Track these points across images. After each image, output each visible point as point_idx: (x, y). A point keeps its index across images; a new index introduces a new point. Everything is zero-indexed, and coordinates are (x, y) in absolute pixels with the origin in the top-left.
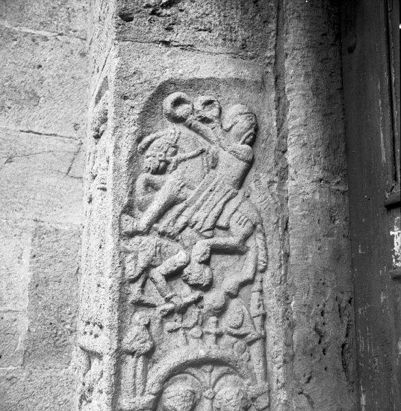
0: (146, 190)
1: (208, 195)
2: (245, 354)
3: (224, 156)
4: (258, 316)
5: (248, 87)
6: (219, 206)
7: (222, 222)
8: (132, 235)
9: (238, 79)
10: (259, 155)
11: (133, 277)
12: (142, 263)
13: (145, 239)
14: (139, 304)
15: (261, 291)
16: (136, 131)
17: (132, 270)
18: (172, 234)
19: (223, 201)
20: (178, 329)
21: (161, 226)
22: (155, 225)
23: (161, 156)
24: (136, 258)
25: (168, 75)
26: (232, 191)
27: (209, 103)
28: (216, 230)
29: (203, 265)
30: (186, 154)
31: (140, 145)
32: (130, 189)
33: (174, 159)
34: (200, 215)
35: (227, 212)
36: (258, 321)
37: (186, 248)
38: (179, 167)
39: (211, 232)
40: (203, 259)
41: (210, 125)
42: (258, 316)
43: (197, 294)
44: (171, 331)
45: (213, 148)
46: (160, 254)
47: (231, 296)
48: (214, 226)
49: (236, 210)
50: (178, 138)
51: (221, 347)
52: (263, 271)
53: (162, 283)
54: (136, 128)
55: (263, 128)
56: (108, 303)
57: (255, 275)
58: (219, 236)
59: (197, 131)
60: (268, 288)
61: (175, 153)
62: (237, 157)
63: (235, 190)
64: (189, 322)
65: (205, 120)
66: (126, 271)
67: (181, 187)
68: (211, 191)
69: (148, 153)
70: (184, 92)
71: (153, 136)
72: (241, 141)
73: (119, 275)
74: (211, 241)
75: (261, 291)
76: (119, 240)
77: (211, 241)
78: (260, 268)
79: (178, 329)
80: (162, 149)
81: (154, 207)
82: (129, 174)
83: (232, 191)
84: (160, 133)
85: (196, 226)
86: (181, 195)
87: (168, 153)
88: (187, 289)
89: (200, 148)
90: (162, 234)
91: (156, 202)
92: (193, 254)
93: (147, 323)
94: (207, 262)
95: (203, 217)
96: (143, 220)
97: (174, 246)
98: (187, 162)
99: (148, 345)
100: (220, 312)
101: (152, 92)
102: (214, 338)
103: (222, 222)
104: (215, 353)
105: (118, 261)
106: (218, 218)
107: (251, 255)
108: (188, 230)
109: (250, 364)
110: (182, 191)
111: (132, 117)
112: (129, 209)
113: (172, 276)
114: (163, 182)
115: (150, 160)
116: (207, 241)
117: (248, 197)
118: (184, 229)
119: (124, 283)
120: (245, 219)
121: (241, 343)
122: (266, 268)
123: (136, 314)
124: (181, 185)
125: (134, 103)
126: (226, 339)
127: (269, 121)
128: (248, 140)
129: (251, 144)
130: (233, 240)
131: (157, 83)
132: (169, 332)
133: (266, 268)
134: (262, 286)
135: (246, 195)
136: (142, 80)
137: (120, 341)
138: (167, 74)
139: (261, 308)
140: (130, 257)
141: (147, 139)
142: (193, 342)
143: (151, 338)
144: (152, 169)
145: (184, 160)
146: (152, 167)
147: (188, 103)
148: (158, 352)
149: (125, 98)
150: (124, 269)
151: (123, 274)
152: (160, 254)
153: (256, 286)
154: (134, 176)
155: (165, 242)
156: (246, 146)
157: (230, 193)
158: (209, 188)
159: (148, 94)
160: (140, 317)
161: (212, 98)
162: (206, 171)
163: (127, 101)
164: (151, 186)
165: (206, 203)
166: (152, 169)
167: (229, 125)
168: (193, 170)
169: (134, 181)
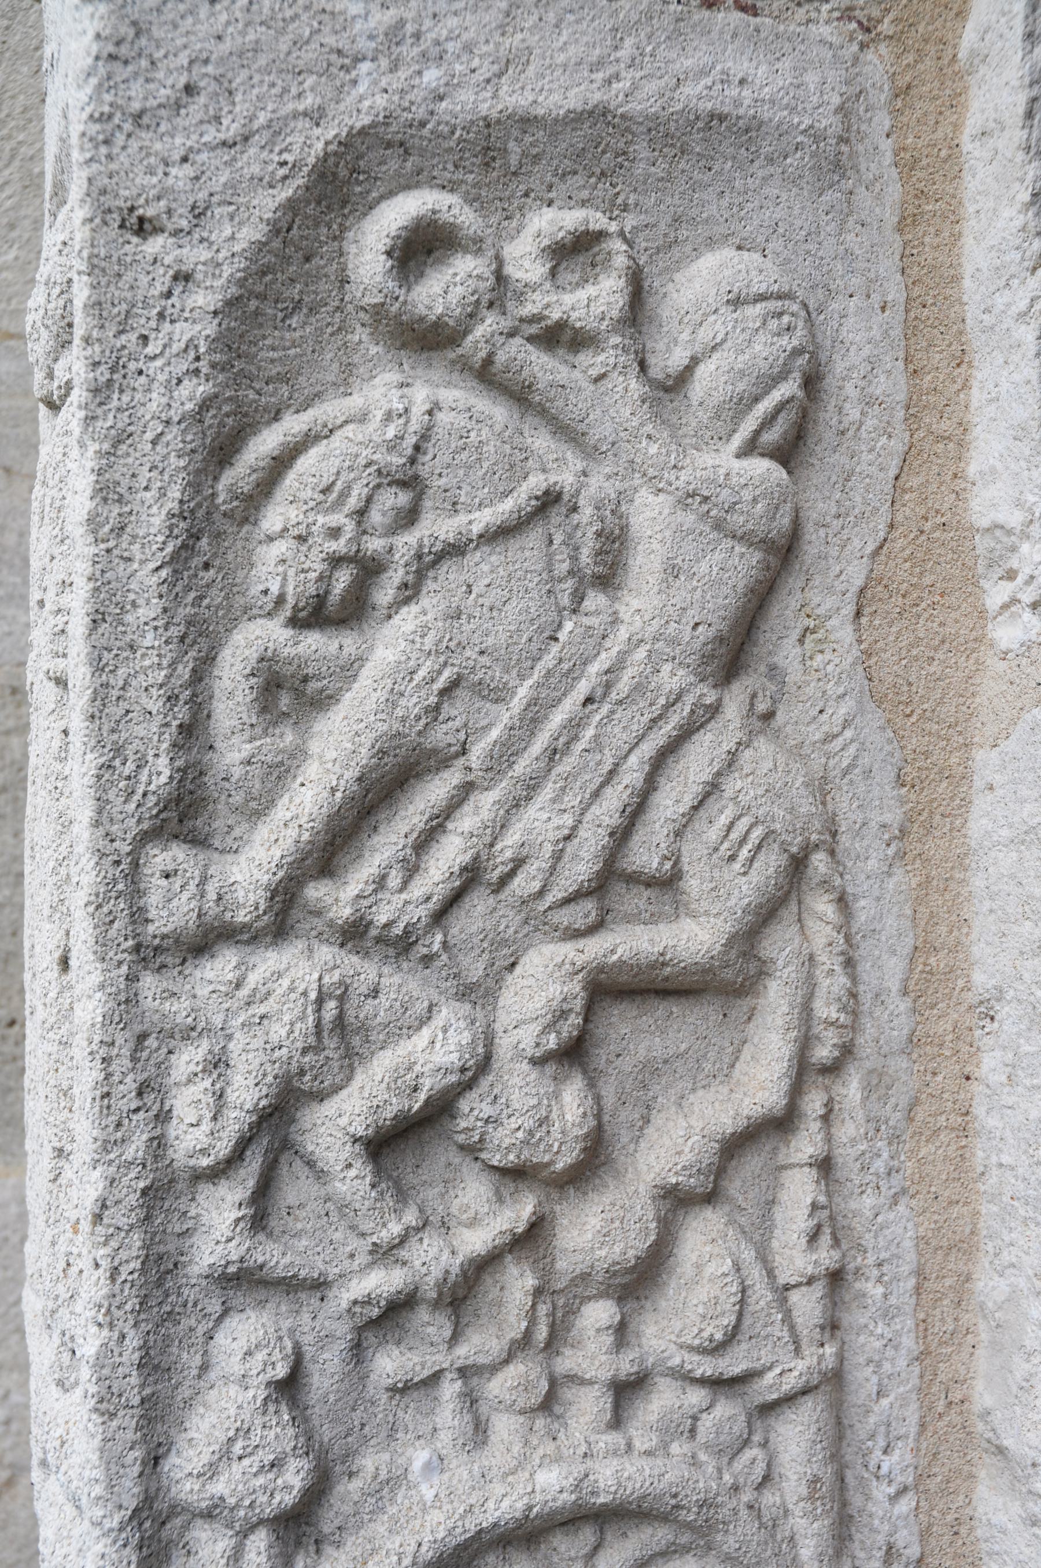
0: (264, 710)
1: (574, 726)
2: (749, 1454)
3: (650, 515)
4: (810, 1281)
5: (770, 160)
6: (633, 774)
7: (645, 855)
8: (204, 940)
9: (722, 118)
10: (819, 506)
11: (205, 1162)
12: (246, 1093)
13: (267, 961)
14: (242, 1282)
15: (825, 1166)
16: (205, 405)
17: (196, 1132)
18: (398, 930)
19: (648, 748)
20: (435, 1378)
21: (339, 897)
22: (315, 892)
23: (335, 533)
24: (217, 1064)
25: (366, 99)
26: (689, 700)
27: (574, 251)
28: (620, 887)
29: (550, 1069)
30: (462, 518)
31: (227, 478)
32: (182, 713)
33: (407, 542)
34: (539, 822)
35: (670, 802)
36: (808, 1306)
37: (466, 992)
38: (430, 585)
39: (589, 906)
40: (552, 1042)
41: (584, 358)
42: (810, 1281)
43: (522, 1210)
44: (402, 1390)
45: (600, 483)
46: (341, 1034)
47: (677, 1201)
48: (610, 877)
49: (712, 788)
50: (425, 436)
51: (639, 1445)
52: (833, 1069)
53: (353, 1180)
54: (203, 389)
55: (845, 371)
56: (93, 1287)
57: (796, 1091)
58: (631, 919)
59: (520, 395)
60: (853, 1141)
61: (409, 517)
62: (718, 526)
63: (703, 688)
64: (481, 1344)
65: (559, 337)
66: (173, 1130)
67: (444, 692)
68: (589, 700)
69: (274, 517)
70: (450, 186)
71: (293, 424)
72: (737, 441)
73: (136, 1148)
74: (595, 949)
75: (825, 1166)
76: (132, 978)
77: (595, 949)
78: (823, 1053)
79: (435, 1378)
80: (345, 494)
81: (306, 803)
82: (175, 631)
83: (689, 700)
84: (330, 409)
85: (518, 881)
86: (441, 736)
87: (376, 517)
88: (474, 1191)
89: (536, 483)
90: (354, 934)
91: (312, 770)
92: (503, 1019)
93: (281, 1371)
94: (573, 1054)
95: (552, 829)
96: (249, 868)
97: (398, 984)
98: (473, 558)
99: (295, 1478)
100: (639, 1281)
101: (286, 193)
102: (607, 1402)
103: (645, 855)
104: (613, 1477)
105: (131, 1083)
106: (622, 835)
107: (777, 998)
108: (479, 903)
109: (769, 1499)
110: (446, 710)
111: (183, 332)
112: (185, 814)
113: (394, 1144)
114: (349, 670)
115: (278, 560)
116: (567, 950)
117: (769, 716)
118: (454, 900)
119: (162, 1193)
120: (757, 833)
121: (726, 1413)
122: (847, 1051)
123: (233, 1322)
124: (441, 683)
125: (194, 255)
126: (664, 1400)
127: (861, 345)
128: (771, 436)
129: (788, 454)
130: (693, 936)
131: (313, 143)
132: (393, 1390)
133: (847, 1051)
134: (829, 1139)
135: (762, 707)
136: (231, 129)
137: (154, 1461)
138: (361, 89)
139: (826, 1239)
140: (187, 1059)
141: (267, 442)
142: (504, 1427)
143: (309, 1443)
144: (291, 601)
145: (455, 550)
146: (298, 588)
147: (476, 246)
148: (348, 1491)
149: (144, 228)
150: (163, 1117)
151: (158, 1144)
152: (341, 1034)
153: (806, 1145)
154: (199, 642)
155: (365, 970)
156: (761, 466)
157: (685, 709)
158: (583, 688)
159: (268, 203)
160: (244, 1345)
161: (598, 220)
162: (565, 600)
163: (155, 245)
164: (287, 694)
165: (566, 765)
166: (291, 601)
167: (678, 358)
168: (500, 595)
169: (200, 675)
